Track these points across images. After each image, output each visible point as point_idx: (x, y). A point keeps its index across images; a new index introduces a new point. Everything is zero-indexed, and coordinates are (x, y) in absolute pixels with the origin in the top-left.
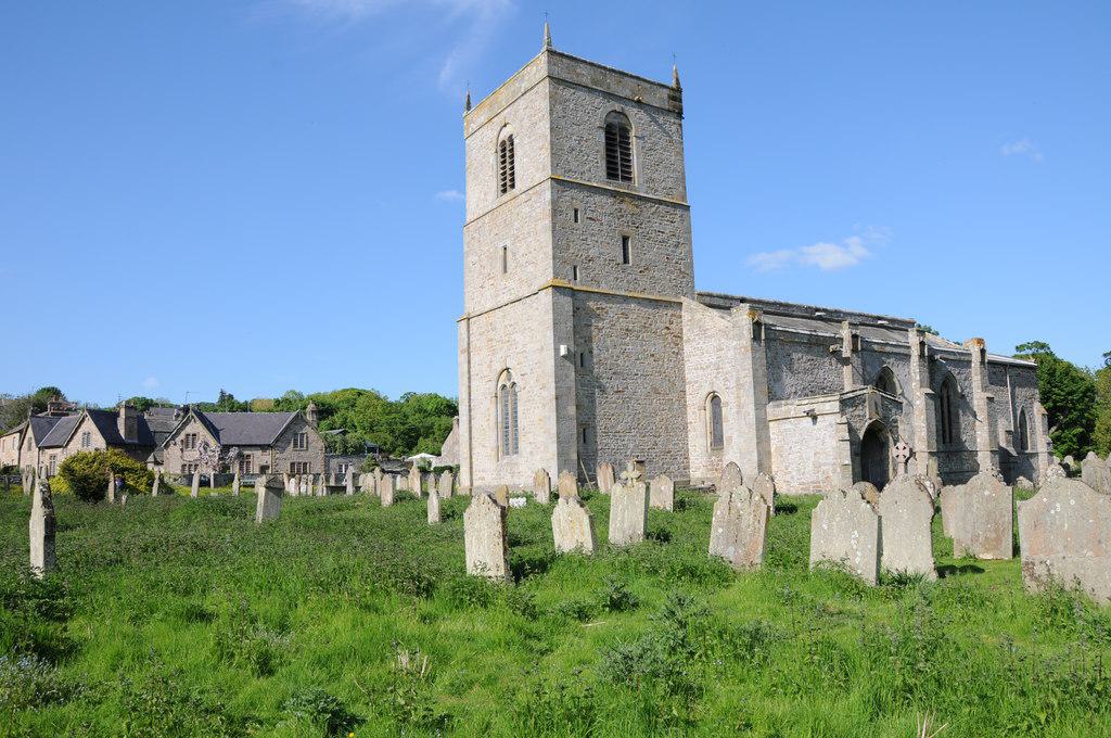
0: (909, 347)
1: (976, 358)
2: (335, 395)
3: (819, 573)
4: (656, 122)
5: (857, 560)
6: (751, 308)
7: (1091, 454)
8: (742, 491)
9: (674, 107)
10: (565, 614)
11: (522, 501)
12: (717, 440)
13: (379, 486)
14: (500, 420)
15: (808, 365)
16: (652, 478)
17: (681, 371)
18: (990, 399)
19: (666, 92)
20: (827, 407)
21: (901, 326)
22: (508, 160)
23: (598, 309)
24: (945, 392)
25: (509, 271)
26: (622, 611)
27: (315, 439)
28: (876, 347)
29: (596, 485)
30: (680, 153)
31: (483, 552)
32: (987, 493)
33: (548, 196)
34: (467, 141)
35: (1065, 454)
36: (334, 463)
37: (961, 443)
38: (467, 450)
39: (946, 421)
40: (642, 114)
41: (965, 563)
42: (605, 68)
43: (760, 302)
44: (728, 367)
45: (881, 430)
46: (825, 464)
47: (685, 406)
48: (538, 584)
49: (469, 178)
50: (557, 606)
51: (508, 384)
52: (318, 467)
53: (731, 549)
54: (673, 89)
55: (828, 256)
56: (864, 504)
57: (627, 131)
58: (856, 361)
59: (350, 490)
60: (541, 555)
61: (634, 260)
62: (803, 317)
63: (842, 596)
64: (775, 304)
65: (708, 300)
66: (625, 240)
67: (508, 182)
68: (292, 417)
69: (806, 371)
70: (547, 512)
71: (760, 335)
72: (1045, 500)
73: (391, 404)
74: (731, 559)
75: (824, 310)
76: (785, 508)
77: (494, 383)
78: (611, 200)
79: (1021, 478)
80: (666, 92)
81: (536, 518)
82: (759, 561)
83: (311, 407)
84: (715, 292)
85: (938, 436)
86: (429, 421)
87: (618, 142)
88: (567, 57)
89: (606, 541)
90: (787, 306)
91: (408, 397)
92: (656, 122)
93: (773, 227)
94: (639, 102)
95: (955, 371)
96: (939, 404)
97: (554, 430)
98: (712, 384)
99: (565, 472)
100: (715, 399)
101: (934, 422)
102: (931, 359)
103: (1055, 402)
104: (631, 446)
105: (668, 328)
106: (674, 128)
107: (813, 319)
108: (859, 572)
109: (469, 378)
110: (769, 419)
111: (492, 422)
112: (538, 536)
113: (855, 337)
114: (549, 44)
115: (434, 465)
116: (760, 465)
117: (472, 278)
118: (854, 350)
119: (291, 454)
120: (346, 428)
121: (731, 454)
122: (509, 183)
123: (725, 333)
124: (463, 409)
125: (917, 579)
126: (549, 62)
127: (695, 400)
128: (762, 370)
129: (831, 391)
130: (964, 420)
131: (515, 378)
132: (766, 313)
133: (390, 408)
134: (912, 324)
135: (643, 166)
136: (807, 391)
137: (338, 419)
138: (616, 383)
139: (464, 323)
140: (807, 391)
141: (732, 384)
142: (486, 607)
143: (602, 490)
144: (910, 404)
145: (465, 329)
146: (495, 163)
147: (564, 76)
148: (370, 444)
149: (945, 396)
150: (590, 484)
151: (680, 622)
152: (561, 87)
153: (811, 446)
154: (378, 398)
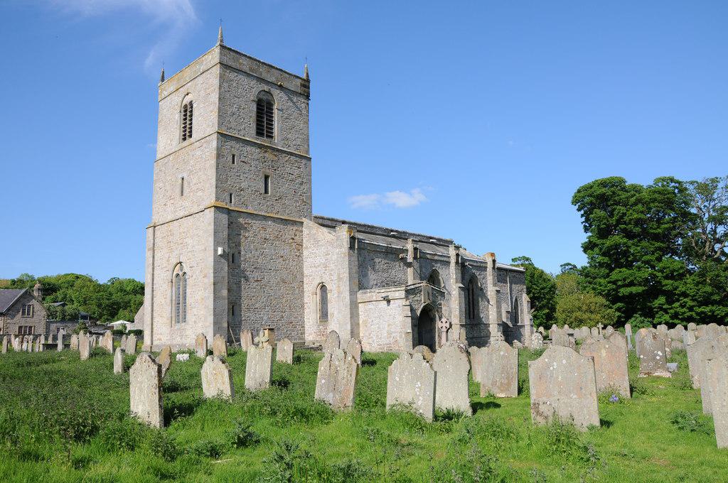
0: (449, 257)
1: (490, 265)
2: (59, 278)
3: (394, 413)
4: (292, 101)
5: (420, 403)
6: (349, 228)
7: (554, 326)
8: (340, 353)
9: (304, 91)
10: (200, 453)
11: (186, 356)
12: (324, 315)
13: (82, 343)
14: (174, 298)
15: (385, 267)
16: (279, 340)
17: (301, 268)
18: (498, 292)
19: (299, 81)
20: (397, 295)
21: (445, 243)
22: (188, 118)
23: (245, 223)
24: (471, 286)
25: (185, 194)
26: (247, 447)
27: (39, 311)
28: (428, 256)
29: (240, 345)
30: (307, 123)
31: (144, 403)
32: (502, 353)
33: (214, 144)
34: (160, 103)
35: (538, 326)
36: (53, 327)
37: (480, 319)
38: (149, 319)
39: (471, 306)
40: (282, 94)
41: (488, 401)
42: (259, 61)
43: (355, 224)
44: (332, 266)
45: (431, 310)
46: (395, 332)
47: (303, 292)
48: (184, 425)
49: (160, 129)
50: (194, 446)
51: (181, 273)
52: (41, 329)
53: (331, 395)
54: (304, 80)
55: (401, 199)
56: (425, 363)
57: (272, 105)
58: (416, 265)
59: (60, 347)
60: (189, 401)
61: (272, 192)
62: (383, 235)
63: (410, 431)
64: (365, 226)
65: (321, 221)
66: (266, 177)
67: (187, 133)
68: (22, 293)
69: (384, 271)
70: (201, 363)
71: (354, 246)
72: (546, 360)
73: (100, 285)
74: (331, 402)
75: (396, 231)
76: (368, 362)
77: (171, 273)
78: (258, 150)
79: (515, 341)
80: (299, 82)
81: (192, 370)
82: (350, 404)
83: (37, 285)
84: (326, 216)
85: (466, 314)
86: (127, 298)
87: (264, 112)
88: (234, 51)
89: (242, 386)
90: (373, 227)
91: (113, 281)
92: (292, 101)
93: (365, 176)
94: (281, 86)
95: (477, 273)
96: (467, 293)
97: (211, 307)
98: (321, 277)
99: (218, 335)
100: (323, 288)
101: (463, 305)
102: (463, 265)
103: (534, 293)
104: (265, 318)
105: (293, 239)
106: (303, 105)
107: (390, 236)
108: (421, 411)
109: (153, 268)
110: (359, 301)
111: (168, 300)
112: (194, 382)
113: (415, 249)
114: (222, 41)
115: (128, 329)
116: (352, 333)
117: (158, 198)
118: (415, 258)
119: (19, 320)
120: (66, 300)
121: (333, 325)
122: (188, 134)
123: (330, 243)
124: (148, 290)
125: (459, 415)
126: (221, 53)
127: (310, 288)
128: (355, 269)
129: (400, 284)
130: (482, 304)
131: (185, 270)
132: (359, 231)
133: (99, 288)
134: (451, 242)
135: (281, 130)
136: (384, 284)
137: (59, 294)
138: (256, 275)
139: (151, 229)
140: (384, 284)
141: (335, 277)
142: (133, 449)
143: (244, 349)
144: (449, 293)
145: (152, 233)
146: (179, 119)
147: (230, 64)
148: (83, 313)
149: (471, 289)
150: (236, 344)
151: (287, 464)
152: (228, 71)
153: (386, 321)
154: (91, 281)
